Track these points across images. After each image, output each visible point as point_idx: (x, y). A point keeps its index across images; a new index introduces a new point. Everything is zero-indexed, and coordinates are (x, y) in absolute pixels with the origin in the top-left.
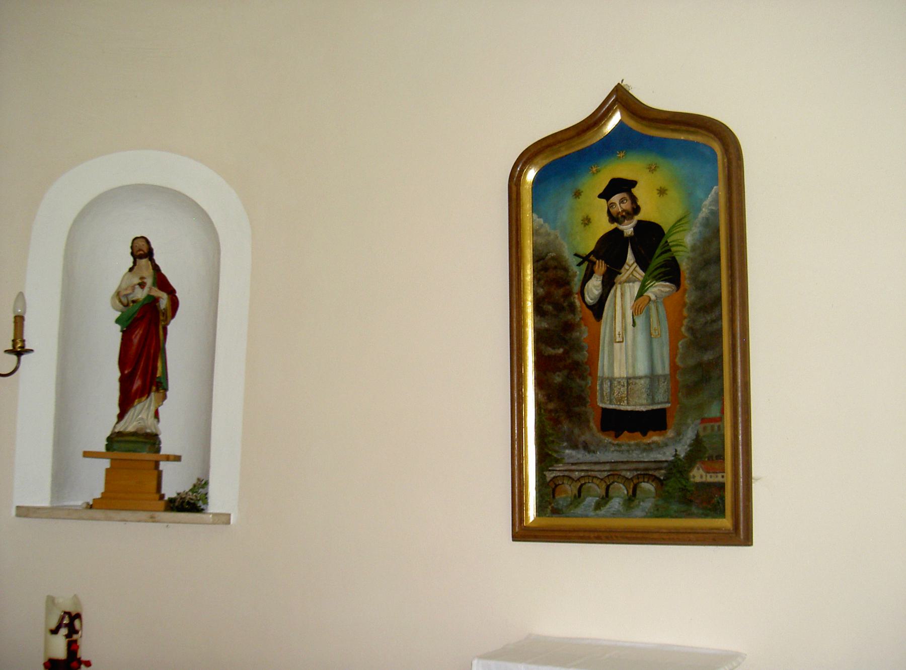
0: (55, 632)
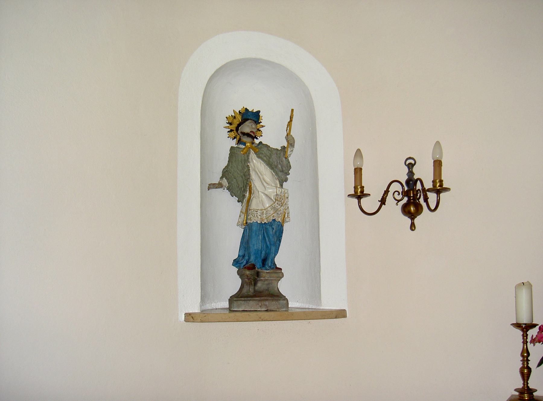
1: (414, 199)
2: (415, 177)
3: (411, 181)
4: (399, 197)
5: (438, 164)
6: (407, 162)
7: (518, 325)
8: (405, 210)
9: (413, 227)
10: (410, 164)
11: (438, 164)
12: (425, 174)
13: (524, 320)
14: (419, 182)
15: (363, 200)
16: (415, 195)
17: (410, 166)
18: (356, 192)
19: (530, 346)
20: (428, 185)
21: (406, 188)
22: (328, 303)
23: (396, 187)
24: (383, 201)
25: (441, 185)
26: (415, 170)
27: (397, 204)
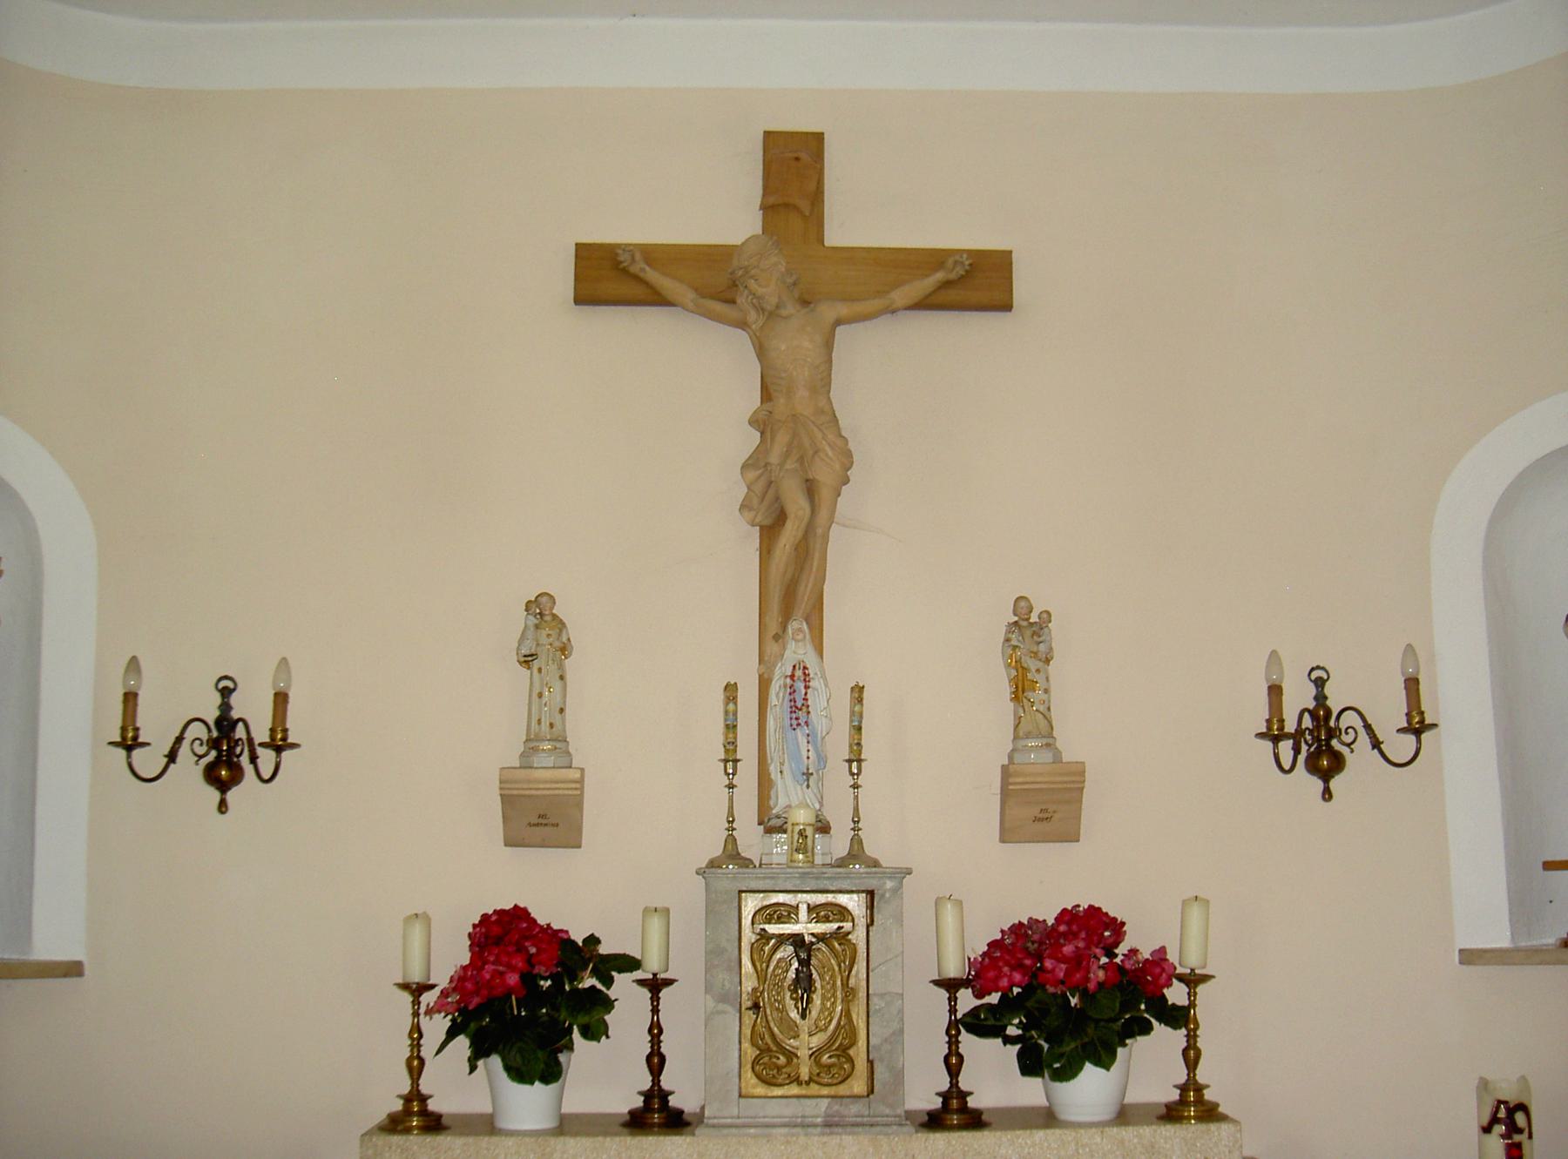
0: (1487, 1130)
1: (226, 756)
2: (235, 714)
3: (225, 723)
4: (201, 750)
5: (281, 699)
6: (221, 685)
7: (405, 986)
8: (211, 774)
9: (223, 807)
10: (225, 688)
11: (281, 699)
12: (254, 712)
13: (416, 977)
14: (240, 725)
15: (136, 753)
16: (231, 750)
17: (226, 693)
18: (124, 738)
19: (424, 1021)
20: (261, 734)
21: (215, 734)
22: (47, 946)
23: (197, 730)
24: (172, 757)
25: (284, 739)
26: (234, 699)
27: (197, 763)
